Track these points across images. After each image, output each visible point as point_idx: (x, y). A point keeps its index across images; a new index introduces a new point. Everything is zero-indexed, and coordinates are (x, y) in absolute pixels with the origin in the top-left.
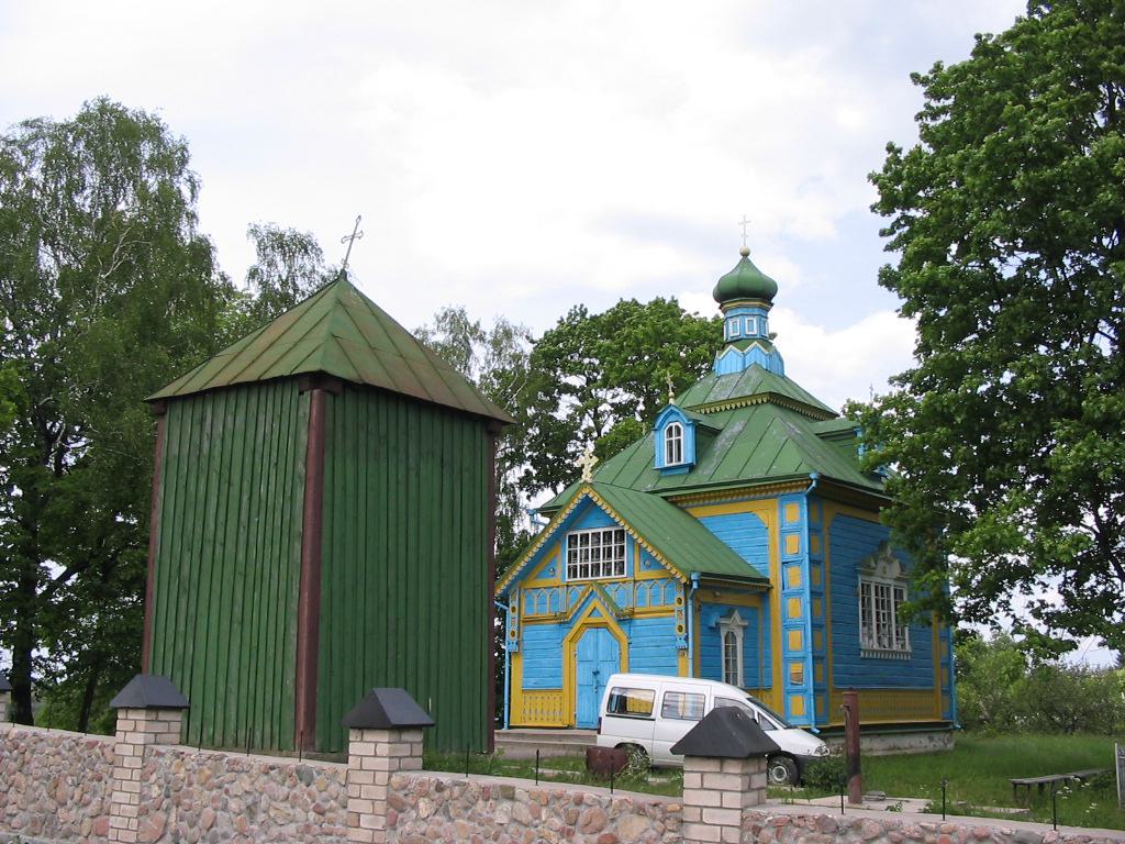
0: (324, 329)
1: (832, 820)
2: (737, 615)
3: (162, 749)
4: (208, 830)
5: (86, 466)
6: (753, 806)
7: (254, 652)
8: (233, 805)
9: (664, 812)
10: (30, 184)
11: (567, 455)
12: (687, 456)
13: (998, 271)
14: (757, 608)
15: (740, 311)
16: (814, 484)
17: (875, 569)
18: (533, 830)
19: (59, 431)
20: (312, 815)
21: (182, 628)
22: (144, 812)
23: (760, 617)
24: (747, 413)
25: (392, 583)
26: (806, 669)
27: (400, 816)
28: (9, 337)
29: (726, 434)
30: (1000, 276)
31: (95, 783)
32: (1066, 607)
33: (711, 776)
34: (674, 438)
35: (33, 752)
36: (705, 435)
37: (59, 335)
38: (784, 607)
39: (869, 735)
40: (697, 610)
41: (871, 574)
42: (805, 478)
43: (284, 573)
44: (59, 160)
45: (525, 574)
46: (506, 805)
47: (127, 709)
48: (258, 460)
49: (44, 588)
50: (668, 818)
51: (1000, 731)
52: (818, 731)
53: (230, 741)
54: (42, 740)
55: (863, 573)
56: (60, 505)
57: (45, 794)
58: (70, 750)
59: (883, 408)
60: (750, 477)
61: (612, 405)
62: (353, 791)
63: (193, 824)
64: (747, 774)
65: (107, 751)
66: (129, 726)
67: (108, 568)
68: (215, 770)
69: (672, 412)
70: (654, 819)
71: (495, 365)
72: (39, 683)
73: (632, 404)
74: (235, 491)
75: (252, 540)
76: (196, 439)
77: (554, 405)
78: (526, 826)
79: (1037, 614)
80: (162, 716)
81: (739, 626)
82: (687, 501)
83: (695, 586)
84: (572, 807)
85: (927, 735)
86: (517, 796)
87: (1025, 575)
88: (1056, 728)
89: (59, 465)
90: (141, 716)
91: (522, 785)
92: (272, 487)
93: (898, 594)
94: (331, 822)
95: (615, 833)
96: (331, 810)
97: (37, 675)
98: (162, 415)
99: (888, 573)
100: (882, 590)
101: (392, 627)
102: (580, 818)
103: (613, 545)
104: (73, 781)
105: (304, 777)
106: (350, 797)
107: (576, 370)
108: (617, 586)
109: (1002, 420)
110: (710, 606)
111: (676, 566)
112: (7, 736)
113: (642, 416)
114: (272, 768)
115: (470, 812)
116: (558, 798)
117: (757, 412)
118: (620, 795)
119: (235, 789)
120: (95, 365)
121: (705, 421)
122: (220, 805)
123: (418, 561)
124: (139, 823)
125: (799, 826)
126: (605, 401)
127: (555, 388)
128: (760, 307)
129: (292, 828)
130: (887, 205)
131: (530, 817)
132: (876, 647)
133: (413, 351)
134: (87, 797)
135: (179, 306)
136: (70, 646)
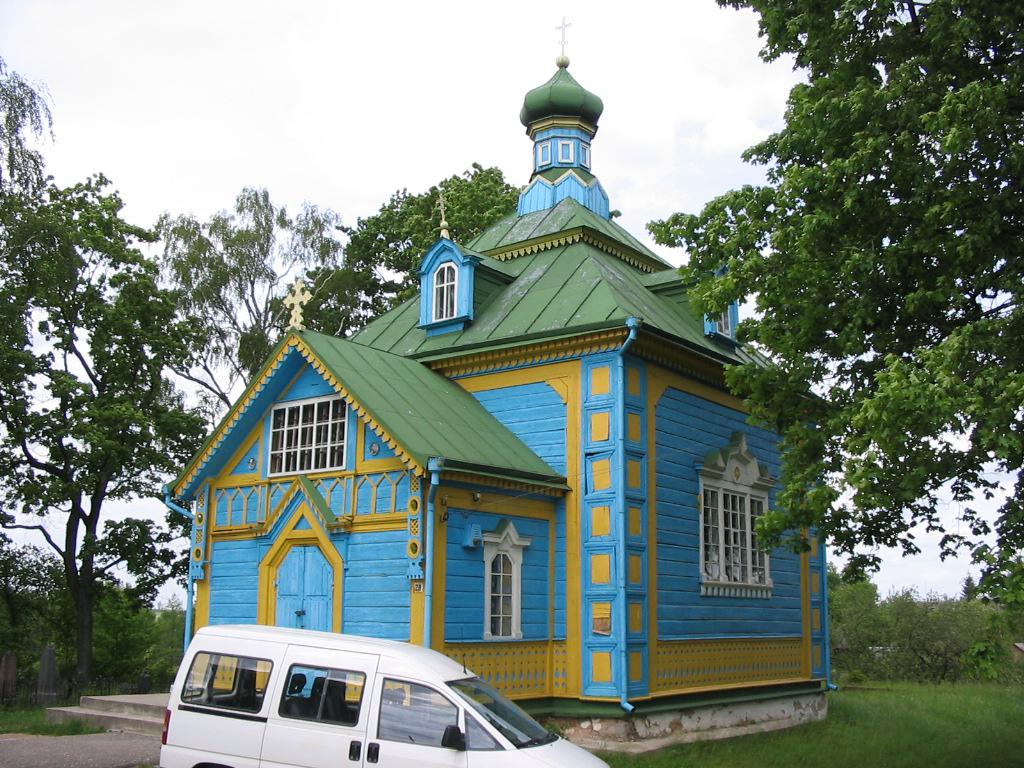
2: (511, 530)
12: (462, 306)
15: (552, 133)
16: (632, 335)
26: (615, 612)
29: (521, 282)
36: (490, 282)
38: (586, 518)
39: (711, 706)
40: (442, 520)
41: (718, 478)
69: (445, 249)
81: (515, 546)
82: (457, 368)
83: (434, 480)
85: (791, 702)
93: (756, 506)
99: (741, 477)
100: (732, 500)
108: (333, 483)
110: (466, 514)
128: (579, 128)
132: (723, 579)
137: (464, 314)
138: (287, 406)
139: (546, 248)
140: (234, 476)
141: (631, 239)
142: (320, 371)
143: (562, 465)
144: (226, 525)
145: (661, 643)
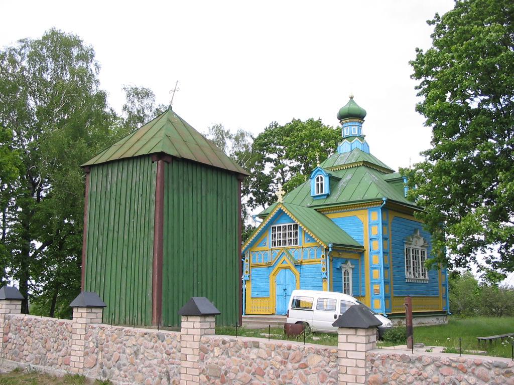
0: (163, 133)
1: (408, 356)
2: (349, 263)
3: (94, 325)
4: (116, 362)
5: (51, 197)
6: (371, 350)
7: (133, 281)
8: (128, 351)
9: (329, 353)
10: (23, 69)
11: (269, 191)
12: (326, 190)
13: (469, 105)
14: (358, 260)
15: (349, 124)
16: (384, 203)
17: (412, 242)
18: (268, 362)
19: (38, 182)
20: (165, 355)
21: (99, 270)
22: (86, 354)
23: (360, 264)
24: (353, 170)
25: (195, 249)
26: (381, 287)
27: (206, 355)
28: (15, 139)
29: (344, 180)
30: (470, 107)
31: (64, 341)
32: (501, 260)
33: (352, 336)
34: (320, 182)
35: (35, 327)
36: (334, 181)
37: (38, 137)
38: (371, 259)
40: (331, 261)
41: (410, 244)
42: (379, 201)
43: (146, 246)
44: (35, 57)
45: (252, 245)
46: (255, 350)
47: (78, 307)
48: (133, 192)
49: (33, 253)
50: (331, 356)
51: (468, 315)
52: (386, 316)
53: (122, 321)
54: (39, 322)
55: (407, 244)
56: (38, 215)
57: (41, 346)
58: (52, 326)
59: (417, 169)
60: (355, 200)
61: (290, 167)
62: (183, 344)
63: (109, 360)
64: (368, 335)
65: (69, 327)
66: (79, 315)
67: (62, 244)
68: (119, 335)
70: (325, 356)
71: (236, 150)
72: (31, 296)
73: (299, 167)
74: (122, 208)
75: (131, 230)
76: (104, 184)
77: (263, 167)
78: (265, 360)
79: (488, 262)
80: (94, 310)
82: (326, 211)
83: (330, 250)
84: (286, 351)
86: (260, 346)
87: (482, 244)
88: (493, 314)
89: (38, 197)
90: (84, 310)
91: (262, 341)
92: (140, 206)
93: (423, 253)
94: (173, 358)
95: (306, 363)
96: (173, 353)
97: (30, 292)
98: (88, 173)
99: (418, 243)
101: (195, 268)
102: (290, 356)
103: (292, 231)
104: (53, 340)
105: (161, 338)
106: (182, 347)
107: (273, 151)
109: (473, 173)
110: (337, 259)
111: (322, 241)
112: (23, 320)
113: (303, 172)
114: (145, 334)
115: (238, 353)
116: (280, 347)
117: (358, 170)
118: (308, 345)
119: (129, 343)
120: (54, 151)
121: (334, 174)
122: (121, 351)
123: (207, 239)
124: (84, 359)
125: (392, 359)
126: (286, 165)
127: (262, 160)
128: (359, 122)
129: (155, 361)
130: (418, 75)
131: (266, 355)
133: (203, 142)
134: (60, 347)
135: (92, 123)
136: (44, 279)
137: (327, 193)
138: (277, 226)
139: (353, 167)
140: (258, 247)
141: (377, 161)
142: (290, 216)
143: (362, 243)
144: (256, 263)
145: (395, 297)
